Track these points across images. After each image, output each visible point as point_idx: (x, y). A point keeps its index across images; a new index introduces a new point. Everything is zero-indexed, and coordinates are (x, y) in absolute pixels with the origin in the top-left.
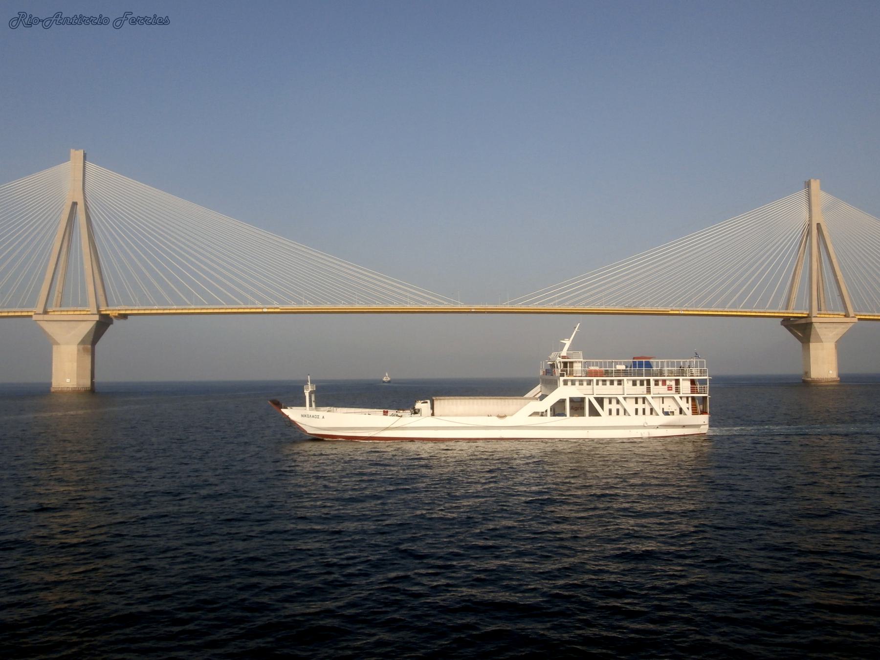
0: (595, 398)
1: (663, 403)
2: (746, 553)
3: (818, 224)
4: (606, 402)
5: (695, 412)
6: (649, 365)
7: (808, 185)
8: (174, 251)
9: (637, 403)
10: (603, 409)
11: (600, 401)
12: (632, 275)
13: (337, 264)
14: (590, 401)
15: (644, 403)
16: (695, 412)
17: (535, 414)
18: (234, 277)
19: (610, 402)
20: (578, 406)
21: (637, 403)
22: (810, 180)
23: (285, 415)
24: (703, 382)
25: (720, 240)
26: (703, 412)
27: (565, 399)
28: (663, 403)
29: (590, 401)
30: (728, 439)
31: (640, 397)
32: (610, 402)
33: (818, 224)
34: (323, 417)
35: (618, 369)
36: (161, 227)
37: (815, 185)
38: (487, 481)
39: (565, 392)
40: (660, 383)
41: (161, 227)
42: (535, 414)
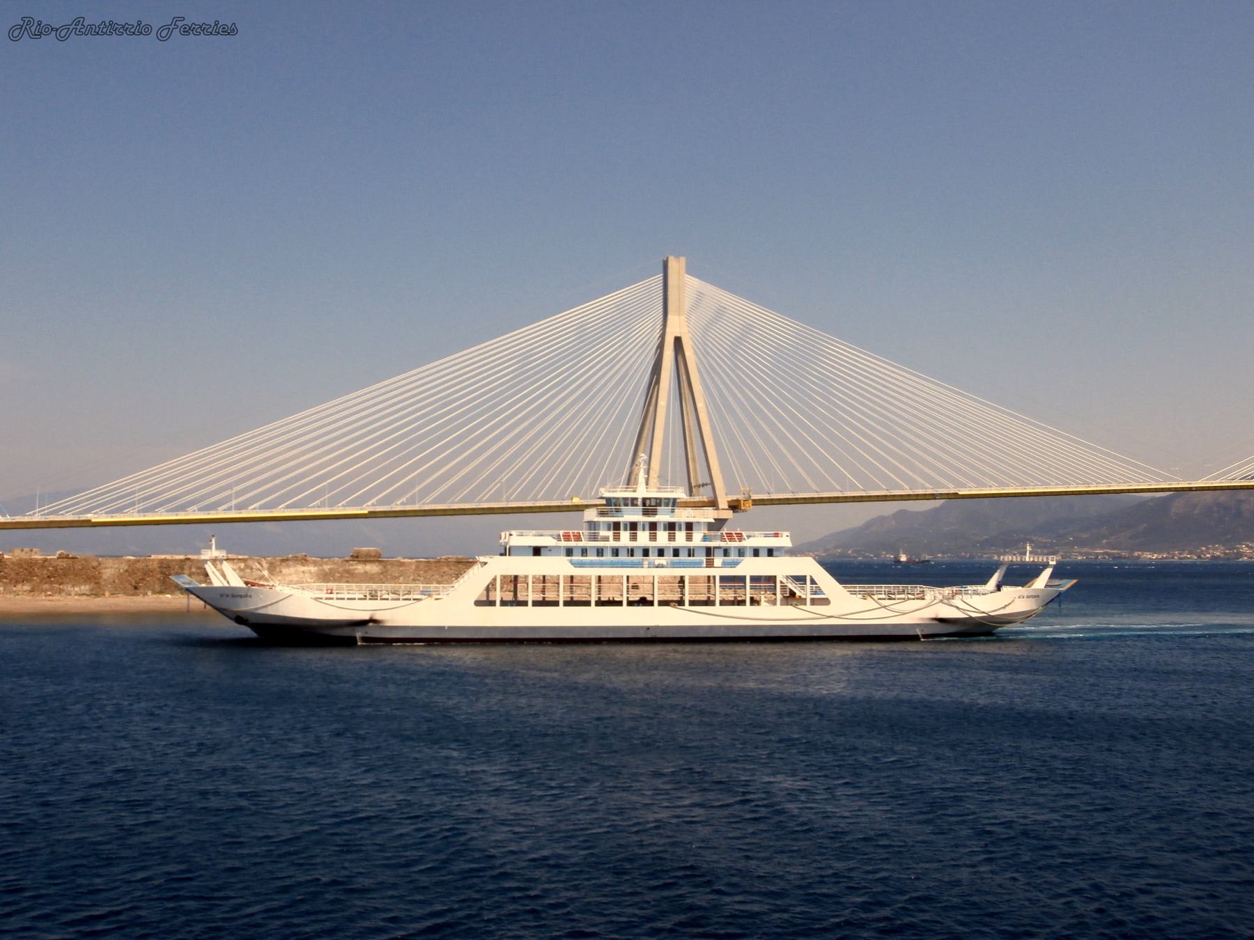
3: (678, 341)
7: (665, 265)
22: (667, 258)
33: (678, 341)
37: (675, 266)
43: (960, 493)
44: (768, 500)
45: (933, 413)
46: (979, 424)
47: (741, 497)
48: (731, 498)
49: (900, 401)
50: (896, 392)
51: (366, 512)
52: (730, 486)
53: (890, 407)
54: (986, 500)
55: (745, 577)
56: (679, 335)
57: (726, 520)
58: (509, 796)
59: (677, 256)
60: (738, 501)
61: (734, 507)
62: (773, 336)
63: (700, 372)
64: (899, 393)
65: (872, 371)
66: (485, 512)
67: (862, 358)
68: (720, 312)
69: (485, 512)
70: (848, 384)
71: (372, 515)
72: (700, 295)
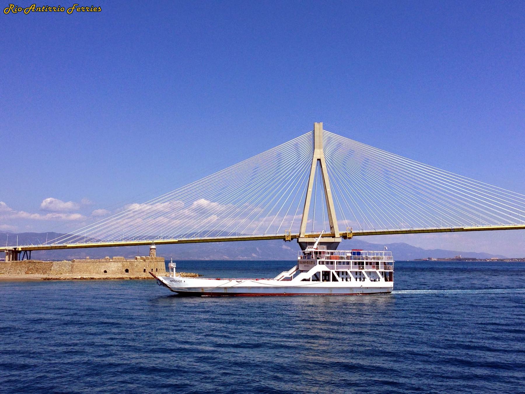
0: (336, 271)
4: (341, 274)
5: (386, 280)
6: (359, 254)
8: (438, 175)
9: (356, 274)
11: (338, 273)
15: (360, 275)
16: (386, 280)
17: (304, 280)
19: (343, 274)
21: (356, 274)
24: (391, 263)
26: (391, 280)
27: (320, 272)
30: (75, 291)
31: (345, 271)
32: (343, 274)
35: (348, 255)
36: (408, 164)
40: (369, 264)
41: (408, 164)
42: (304, 280)
43: (464, 228)
44: (447, 229)
48: (342, 232)
49: (395, 160)
53: (415, 172)
54: (43, 252)
56: (319, 158)
57: (339, 242)
58: (476, 285)
59: (319, 122)
60: (346, 233)
61: (344, 236)
63: (328, 172)
66: (382, 233)
68: (339, 145)
69: (382, 233)
70: (416, 169)
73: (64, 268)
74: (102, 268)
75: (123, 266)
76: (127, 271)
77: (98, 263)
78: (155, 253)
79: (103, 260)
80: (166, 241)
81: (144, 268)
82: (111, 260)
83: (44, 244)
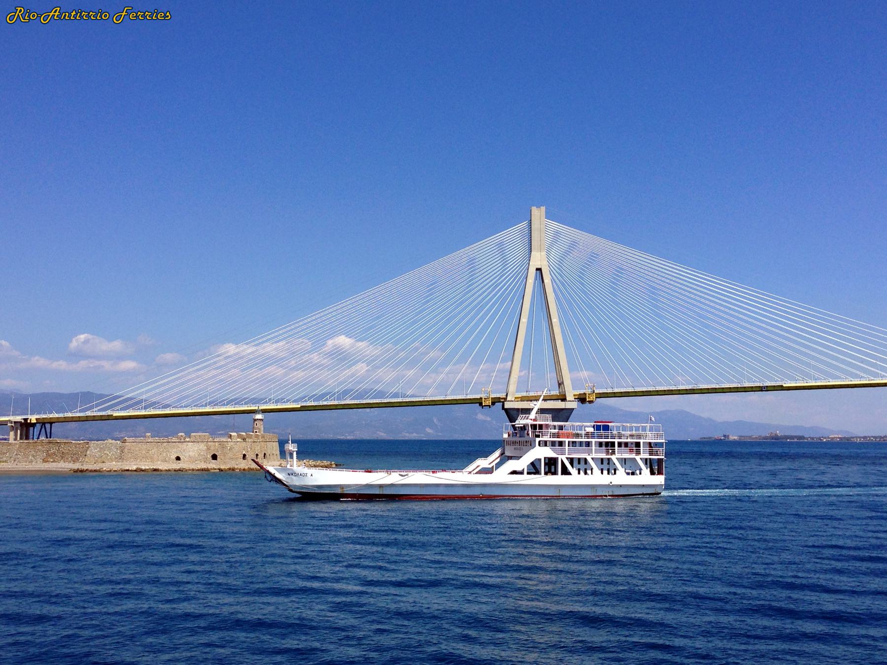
0: (567, 458)
1: (625, 464)
2: (673, 565)
4: (576, 462)
5: (652, 473)
6: (606, 428)
9: (602, 463)
10: (573, 467)
11: (571, 461)
12: (773, 337)
13: (661, 268)
14: (562, 461)
16: (652, 473)
17: (514, 472)
18: (722, 303)
19: (579, 463)
20: (551, 465)
21: (602, 463)
23: (66, 394)
24: (661, 445)
25: (686, 275)
26: (660, 473)
28: (625, 464)
29: (562, 461)
32: (579, 463)
34: (312, 475)
38: (523, 539)
39: (540, 453)
40: (623, 445)
42: (514, 472)
43: (784, 385)
45: (490, 241)
46: (452, 293)
47: (588, 391)
48: (578, 392)
50: (681, 284)
51: (299, 406)
52: (575, 384)
55: (562, 474)
56: (540, 267)
59: (538, 207)
60: (585, 394)
61: (582, 399)
62: (777, 321)
64: (684, 285)
65: (667, 268)
67: (698, 277)
68: (573, 245)
71: (303, 409)
72: (557, 234)
73: (108, 453)
74: (173, 453)
75: (208, 449)
76: (214, 457)
77: (165, 444)
78: (262, 426)
79: (174, 439)
80: (217, 409)
81: (244, 452)
82: (187, 439)
83: (75, 412)
